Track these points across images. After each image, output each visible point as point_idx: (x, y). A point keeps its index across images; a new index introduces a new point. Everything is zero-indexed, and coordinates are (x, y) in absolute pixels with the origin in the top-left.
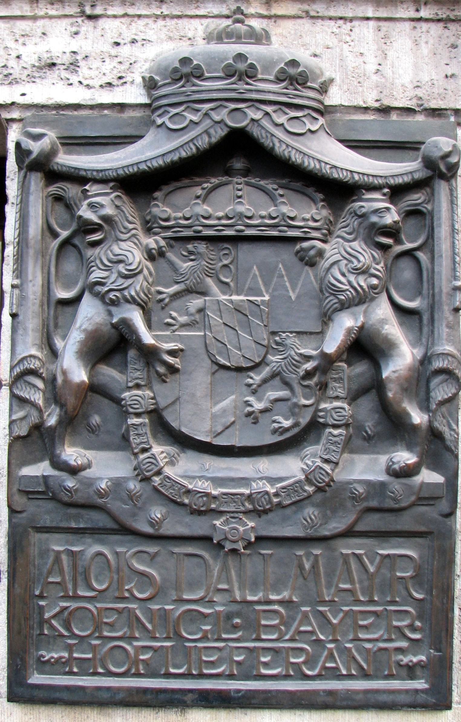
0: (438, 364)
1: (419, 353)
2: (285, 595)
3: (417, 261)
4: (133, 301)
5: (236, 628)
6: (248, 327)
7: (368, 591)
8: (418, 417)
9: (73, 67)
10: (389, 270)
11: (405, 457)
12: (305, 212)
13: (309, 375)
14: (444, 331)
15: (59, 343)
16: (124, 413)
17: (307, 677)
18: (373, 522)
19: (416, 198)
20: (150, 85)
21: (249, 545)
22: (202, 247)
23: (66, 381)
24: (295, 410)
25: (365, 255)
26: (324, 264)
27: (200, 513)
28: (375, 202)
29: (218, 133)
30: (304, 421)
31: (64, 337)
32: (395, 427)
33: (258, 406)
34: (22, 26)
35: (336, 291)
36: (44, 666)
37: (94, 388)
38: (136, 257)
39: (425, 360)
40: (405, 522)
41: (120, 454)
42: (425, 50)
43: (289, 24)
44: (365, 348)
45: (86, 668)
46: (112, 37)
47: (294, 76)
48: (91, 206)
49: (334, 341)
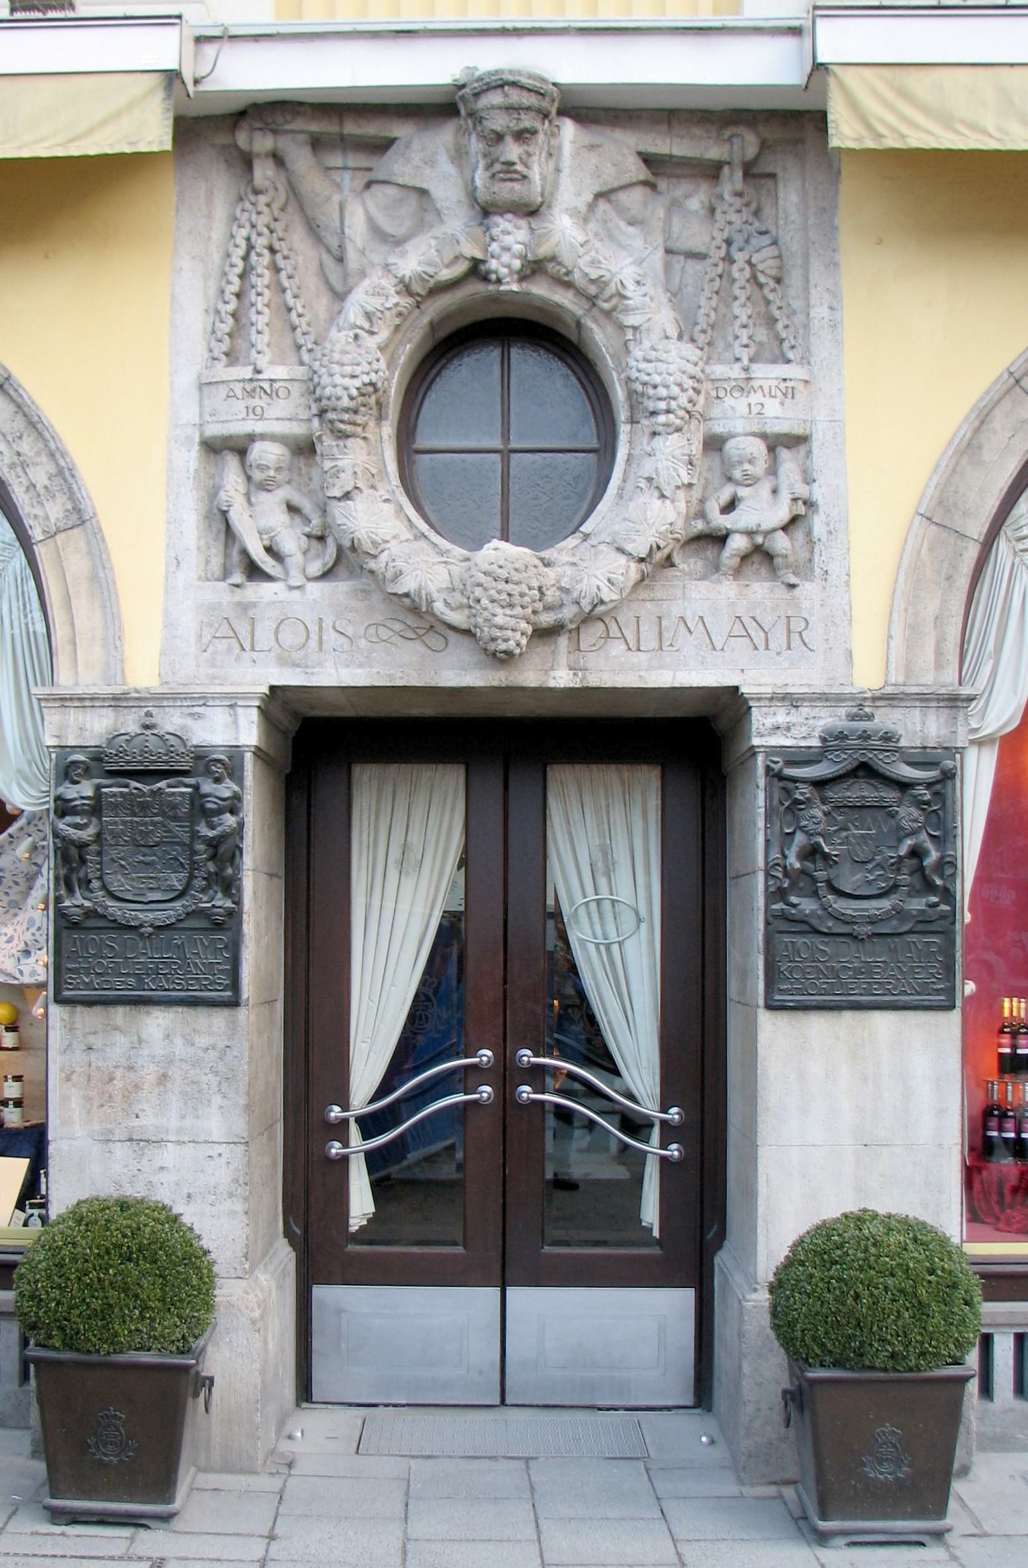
1: (938, 854)
4: (819, 834)
5: (863, 973)
6: (866, 844)
7: (920, 957)
8: (939, 882)
9: (788, 729)
10: (927, 819)
11: (934, 899)
12: (890, 795)
13: (892, 864)
14: (949, 845)
15: (787, 852)
16: (815, 880)
18: (920, 927)
19: (938, 787)
20: (824, 740)
21: (869, 936)
22: (846, 810)
23: (793, 869)
24: (887, 879)
25: (915, 812)
27: (848, 923)
29: (855, 764)
30: (891, 883)
31: (789, 849)
32: (930, 887)
34: (765, 709)
35: (903, 829)
37: (803, 872)
38: (820, 814)
39: (942, 858)
40: (934, 927)
41: (812, 899)
43: (883, 709)
44: (917, 853)
46: (804, 715)
47: (887, 737)
48: (801, 794)
49: (903, 850)
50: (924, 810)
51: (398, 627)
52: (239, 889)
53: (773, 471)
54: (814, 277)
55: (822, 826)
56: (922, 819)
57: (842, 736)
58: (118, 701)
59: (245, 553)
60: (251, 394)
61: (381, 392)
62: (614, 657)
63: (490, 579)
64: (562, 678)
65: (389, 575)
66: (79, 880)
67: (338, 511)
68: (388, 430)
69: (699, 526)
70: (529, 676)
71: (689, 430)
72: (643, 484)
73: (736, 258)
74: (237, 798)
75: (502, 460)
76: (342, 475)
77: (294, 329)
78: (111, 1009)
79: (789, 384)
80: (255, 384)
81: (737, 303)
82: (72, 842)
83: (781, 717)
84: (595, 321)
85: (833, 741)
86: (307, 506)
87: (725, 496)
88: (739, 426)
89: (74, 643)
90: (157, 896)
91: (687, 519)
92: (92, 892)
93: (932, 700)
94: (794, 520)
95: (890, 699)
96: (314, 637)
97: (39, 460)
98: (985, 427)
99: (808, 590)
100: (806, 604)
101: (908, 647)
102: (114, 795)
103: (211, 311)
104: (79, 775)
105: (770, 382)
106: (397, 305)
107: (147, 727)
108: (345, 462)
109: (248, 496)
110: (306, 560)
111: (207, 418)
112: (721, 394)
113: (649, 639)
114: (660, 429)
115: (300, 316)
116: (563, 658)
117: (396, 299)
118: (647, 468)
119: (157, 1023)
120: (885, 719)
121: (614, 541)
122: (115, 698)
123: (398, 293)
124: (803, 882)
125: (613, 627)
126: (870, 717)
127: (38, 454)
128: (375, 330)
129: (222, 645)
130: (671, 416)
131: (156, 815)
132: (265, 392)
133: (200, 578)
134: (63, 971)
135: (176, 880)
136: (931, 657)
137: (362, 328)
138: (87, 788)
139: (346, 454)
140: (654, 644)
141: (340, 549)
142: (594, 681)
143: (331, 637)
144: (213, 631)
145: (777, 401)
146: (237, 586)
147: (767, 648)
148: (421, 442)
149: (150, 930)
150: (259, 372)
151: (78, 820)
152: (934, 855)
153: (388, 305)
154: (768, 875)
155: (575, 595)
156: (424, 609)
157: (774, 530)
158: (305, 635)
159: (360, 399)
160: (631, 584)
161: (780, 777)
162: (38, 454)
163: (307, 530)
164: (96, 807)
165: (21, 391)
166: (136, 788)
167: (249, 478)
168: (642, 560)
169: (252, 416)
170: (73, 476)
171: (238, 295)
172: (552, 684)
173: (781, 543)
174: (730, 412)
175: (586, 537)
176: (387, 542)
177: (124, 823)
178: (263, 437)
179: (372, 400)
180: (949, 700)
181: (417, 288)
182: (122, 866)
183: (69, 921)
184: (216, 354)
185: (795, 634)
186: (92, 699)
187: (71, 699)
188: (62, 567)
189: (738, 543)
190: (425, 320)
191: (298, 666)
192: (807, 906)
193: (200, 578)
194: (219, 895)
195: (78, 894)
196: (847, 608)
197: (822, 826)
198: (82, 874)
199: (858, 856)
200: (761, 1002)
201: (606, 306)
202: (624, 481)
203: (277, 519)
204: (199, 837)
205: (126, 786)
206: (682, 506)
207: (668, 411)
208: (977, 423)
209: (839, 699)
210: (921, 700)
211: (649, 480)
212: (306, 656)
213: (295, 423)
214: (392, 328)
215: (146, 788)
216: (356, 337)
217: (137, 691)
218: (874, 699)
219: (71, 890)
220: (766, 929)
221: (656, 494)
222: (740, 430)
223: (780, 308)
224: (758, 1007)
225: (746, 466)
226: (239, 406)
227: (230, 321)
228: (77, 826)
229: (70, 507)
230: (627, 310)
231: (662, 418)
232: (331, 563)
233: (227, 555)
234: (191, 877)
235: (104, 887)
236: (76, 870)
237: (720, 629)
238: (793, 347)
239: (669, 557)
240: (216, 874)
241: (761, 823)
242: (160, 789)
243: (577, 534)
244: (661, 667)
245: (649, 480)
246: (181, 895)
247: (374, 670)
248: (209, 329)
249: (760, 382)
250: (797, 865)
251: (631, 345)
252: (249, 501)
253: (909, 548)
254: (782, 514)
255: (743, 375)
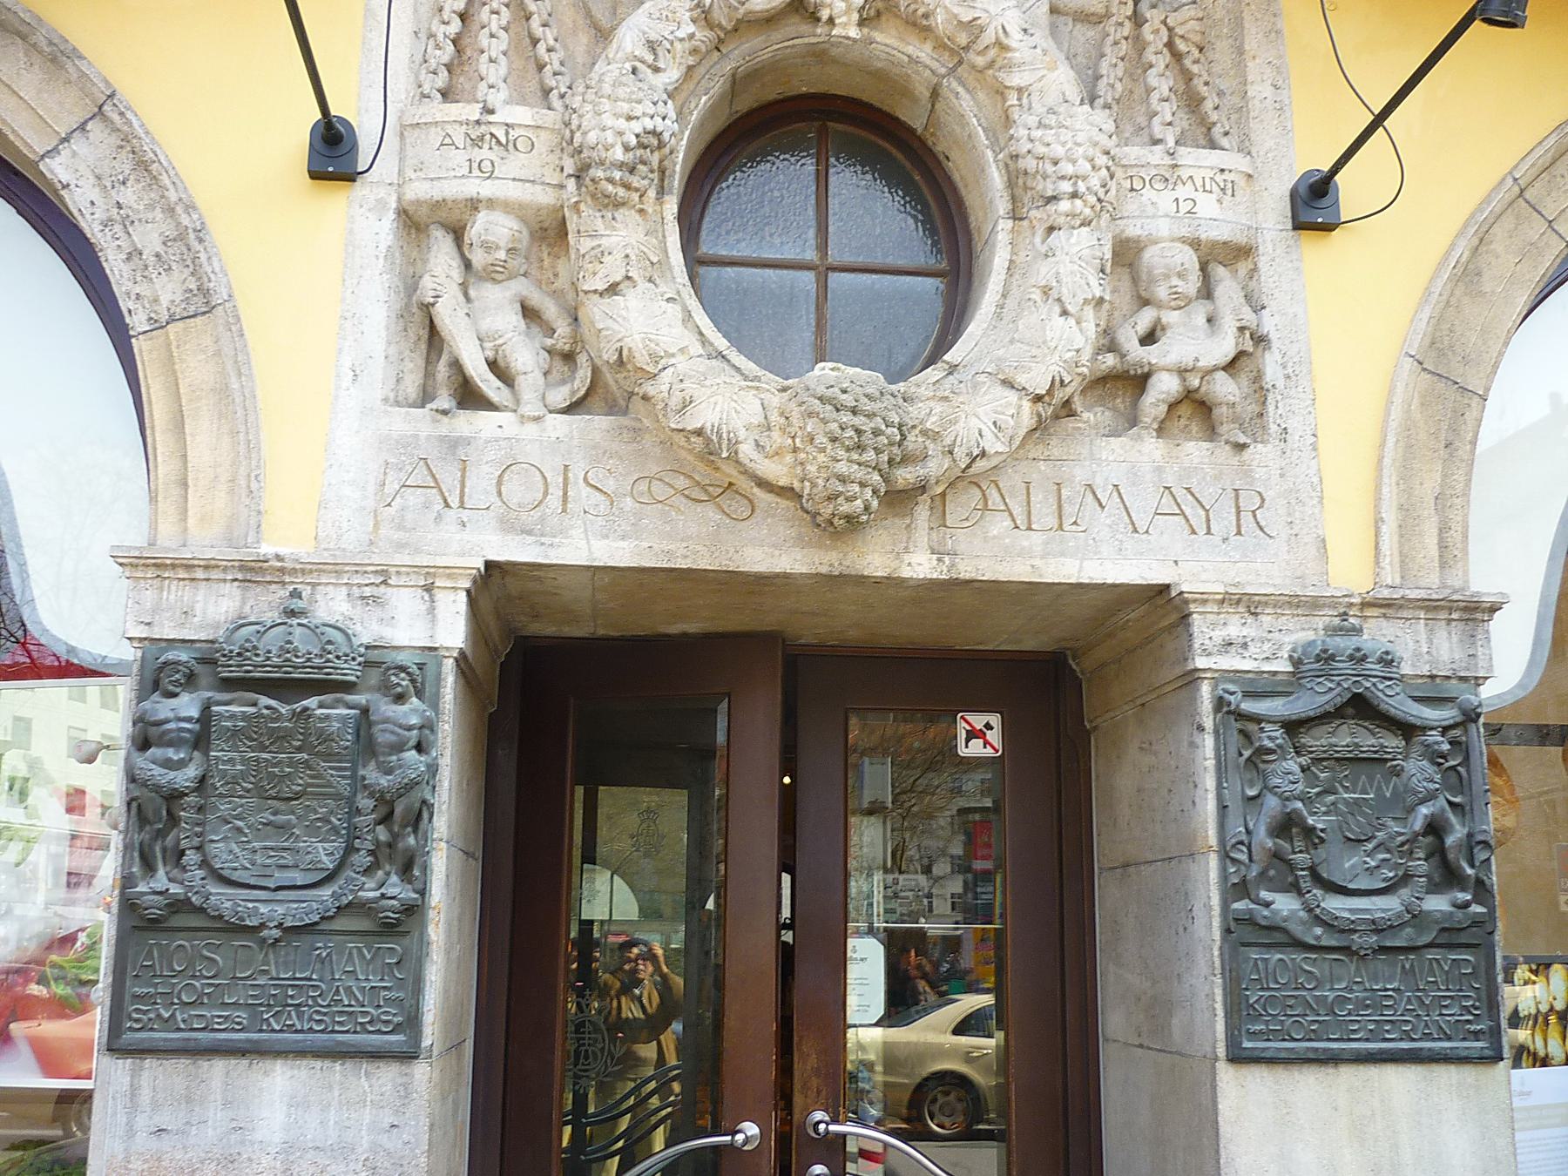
0: (1480, 838)
1: (1465, 831)
2: (1395, 985)
3: (1458, 773)
12: (1393, 742)
13: (1402, 844)
16: (1291, 866)
17: (1414, 1040)
20: (1296, 662)
21: (1375, 951)
26: (1405, 776)
28: (1434, 736)
33: (1373, 864)
36: (1253, 1035)
38: (1296, 769)
39: (1470, 835)
42: (1455, 639)
45: (1266, 1035)
46: (1266, 627)
48: (1270, 738)
49: (1418, 825)
50: (1440, 764)
51: (681, 482)
52: (425, 868)
53: (1207, 292)
54: (1250, 45)
55: (1300, 786)
56: (1437, 777)
57: (1326, 657)
58: (252, 572)
59: (456, 365)
60: (477, 142)
61: (667, 150)
62: (995, 537)
63: (829, 407)
64: (920, 565)
65: (674, 402)
66: (164, 850)
67: (597, 312)
68: (671, 206)
69: (1110, 360)
70: (875, 558)
71: (1098, 228)
72: (1037, 295)
73: (1148, 15)
74: (428, 726)
75: (818, 281)
76: (606, 259)
77: (541, 67)
78: (204, 1064)
79: (1226, 176)
80: (483, 129)
81: (1153, 71)
82: (157, 788)
83: (1235, 628)
84: (962, 83)
85: (1312, 664)
86: (551, 310)
87: (1145, 319)
88: (1163, 228)
89: (185, 485)
90: (299, 878)
91: (1099, 351)
92: (184, 869)
93: (1443, 608)
94: (1240, 355)
95: (1387, 606)
96: (556, 493)
97: (150, 216)
98: (1483, 249)
99: (1260, 454)
100: (1259, 473)
101: (1402, 536)
102: (233, 716)
103: (423, 36)
104: (177, 683)
105: (1203, 173)
106: (692, 36)
107: (292, 613)
108: (613, 239)
109: (464, 287)
110: (547, 385)
111: (410, 174)
112: (1137, 185)
113: (1044, 515)
114: (1061, 220)
115: (549, 50)
116: (922, 535)
117: (691, 28)
118: (1044, 272)
119: (279, 1083)
120: (1378, 634)
121: (1000, 370)
122: (243, 567)
123: (694, 21)
124: (1282, 873)
125: (994, 496)
126: (1358, 631)
127: (151, 207)
128: (661, 65)
129: (413, 498)
130: (1078, 202)
131: (299, 750)
132: (499, 142)
133: (386, 400)
134: (127, 997)
135: (324, 853)
136: (1434, 551)
137: (643, 62)
138: (187, 705)
139: (614, 228)
140: (1052, 521)
141: (596, 371)
142: (966, 571)
143: (582, 495)
144: (403, 476)
145: (1214, 197)
146: (445, 412)
147: (1209, 532)
148: (706, 248)
149: (276, 933)
150: (492, 112)
151: (171, 753)
152: (1456, 834)
153: (681, 34)
154: (1225, 856)
155: (948, 441)
156: (725, 455)
157: (1215, 369)
158: (541, 486)
159: (639, 152)
160: (1023, 432)
161: (1241, 716)
162: (151, 207)
163: (549, 342)
164: (202, 737)
165: (129, 115)
166: (267, 708)
167: (468, 265)
168: (1038, 399)
169: (476, 172)
170: (201, 241)
171: (463, 17)
172: (906, 573)
173: (1225, 388)
174: (1150, 210)
175: (952, 369)
176: (673, 355)
177: (244, 761)
178: (491, 203)
179: (655, 159)
180: (1465, 609)
181: (719, 16)
182: (239, 830)
183: (142, 917)
184: (426, 89)
185: (1247, 514)
186: (206, 567)
187: (174, 566)
188: (174, 372)
189: (1165, 386)
190: (728, 67)
191: (530, 533)
192: (1285, 905)
193: (386, 400)
194: (394, 878)
195: (161, 872)
196: (1315, 480)
197: (1300, 786)
198: (170, 840)
199: (1351, 831)
200: (1221, 1051)
201: (980, 61)
202: (1004, 296)
203: (507, 322)
204: (365, 787)
205: (255, 705)
206: (1091, 328)
207: (1074, 195)
208: (1476, 241)
209: (1314, 605)
210: (1428, 609)
211: (1046, 291)
212: (542, 519)
213: (539, 188)
214: (683, 69)
215: (284, 709)
216: (634, 71)
217: (279, 558)
218: (1365, 605)
219: (149, 866)
220: (1224, 939)
221: (1057, 309)
222: (1165, 233)
223: (1206, 84)
224: (1216, 1059)
225: (1175, 281)
226: (459, 158)
227: (450, 48)
228: (168, 764)
229: (193, 286)
230: (1009, 66)
231: (1064, 205)
232: (582, 392)
233: (429, 374)
234: (350, 849)
235: (205, 864)
236: (160, 834)
237: (1143, 503)
238: (1226, 134)
239: (1067, 403)
240: (390, 845)
241: (1210, 782)
242: (306, 709)
243: (939, 365)
244: (1063, 554)
245: (1046, 291)
246: (330, 878)
247: (646, 544)
248: (419, 58)
249: (1190, 172)
250: (1270, 843)
251: (1015, 114)
252: (466, 295)
253: (1398, 400)
254: (1224, 347)
255: (1168, 161)
